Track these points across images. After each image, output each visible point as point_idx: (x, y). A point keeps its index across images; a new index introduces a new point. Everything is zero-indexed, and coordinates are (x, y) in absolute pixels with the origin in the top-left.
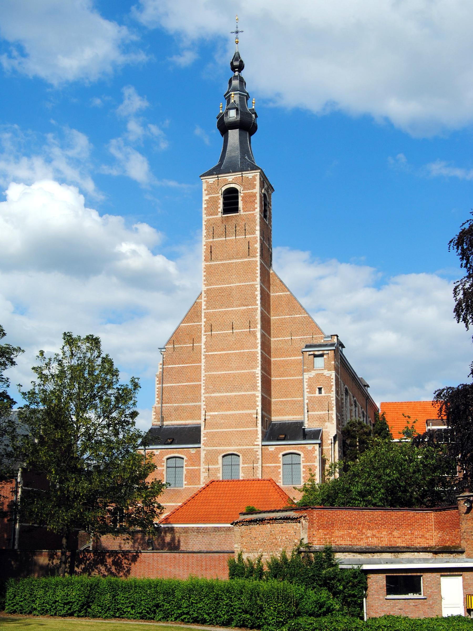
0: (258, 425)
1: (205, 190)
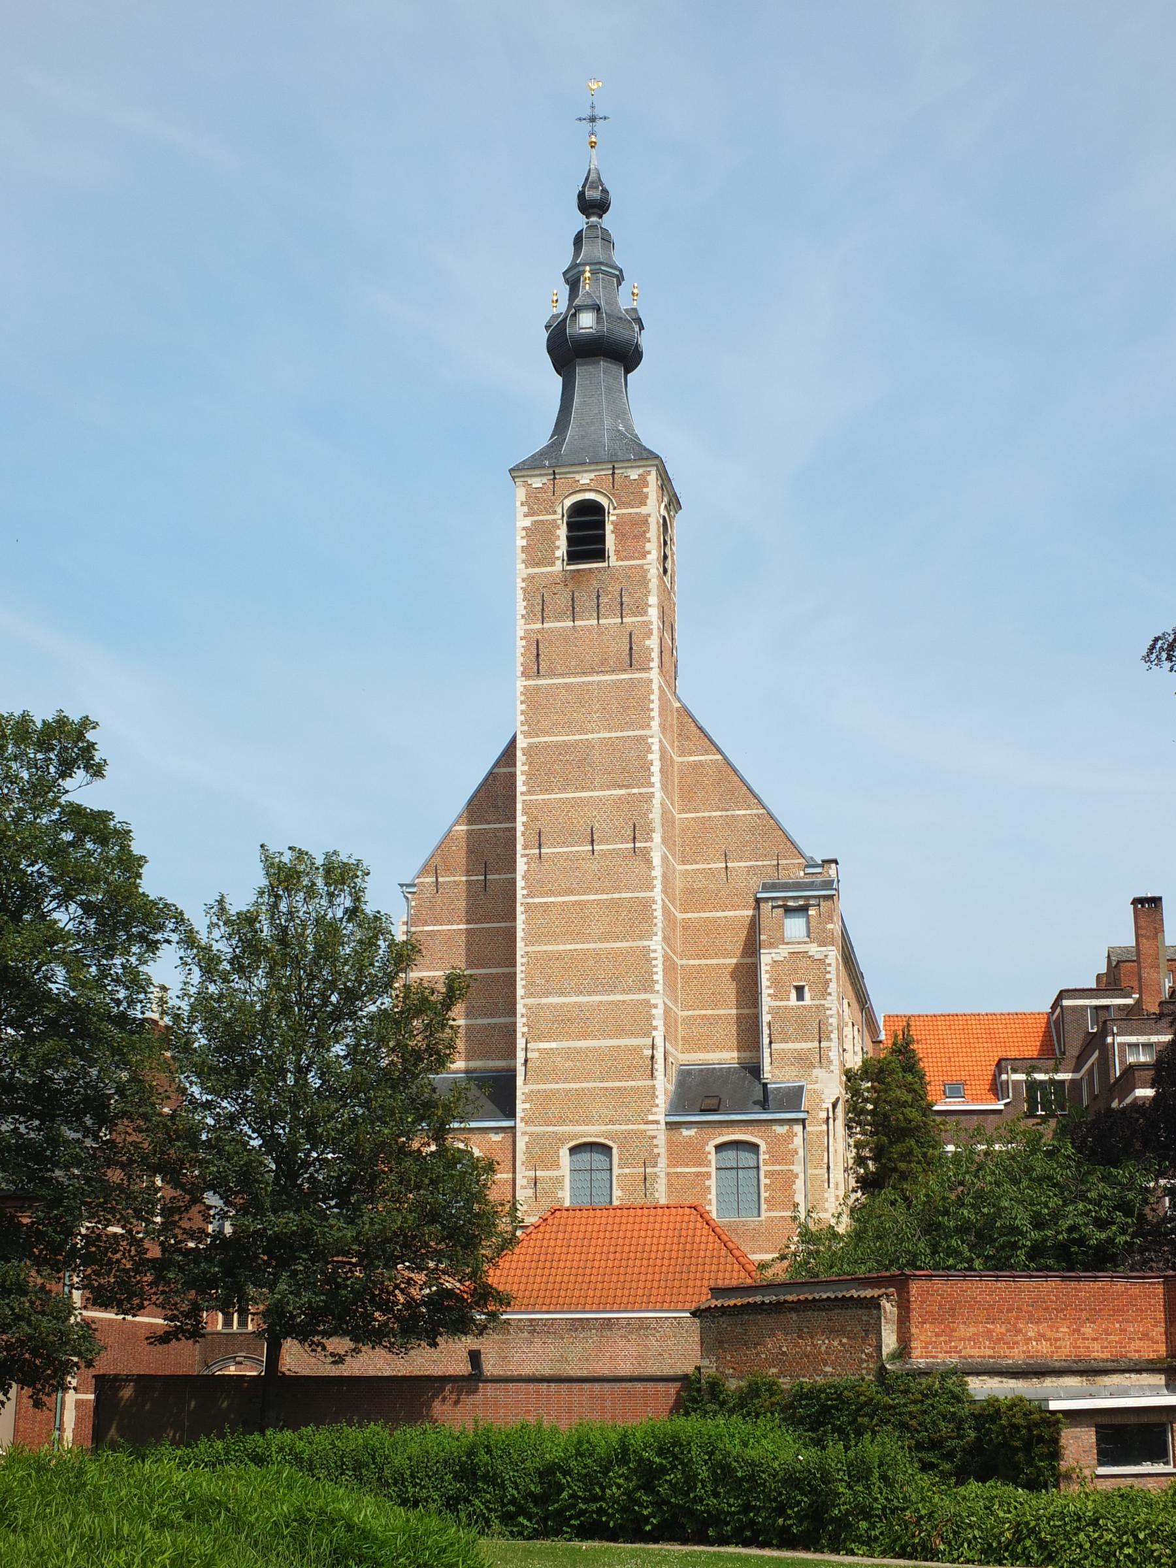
0: (656, 1074)
1: (522, 504)
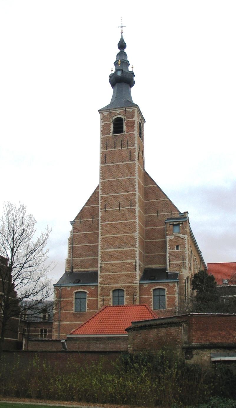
0: (137, 270)
